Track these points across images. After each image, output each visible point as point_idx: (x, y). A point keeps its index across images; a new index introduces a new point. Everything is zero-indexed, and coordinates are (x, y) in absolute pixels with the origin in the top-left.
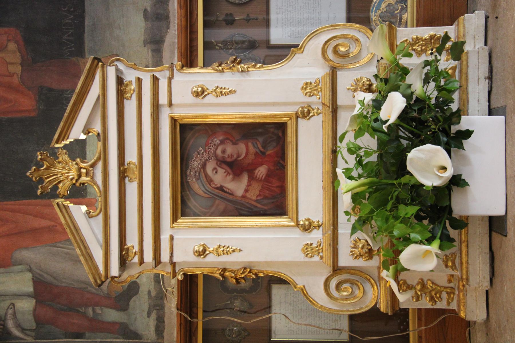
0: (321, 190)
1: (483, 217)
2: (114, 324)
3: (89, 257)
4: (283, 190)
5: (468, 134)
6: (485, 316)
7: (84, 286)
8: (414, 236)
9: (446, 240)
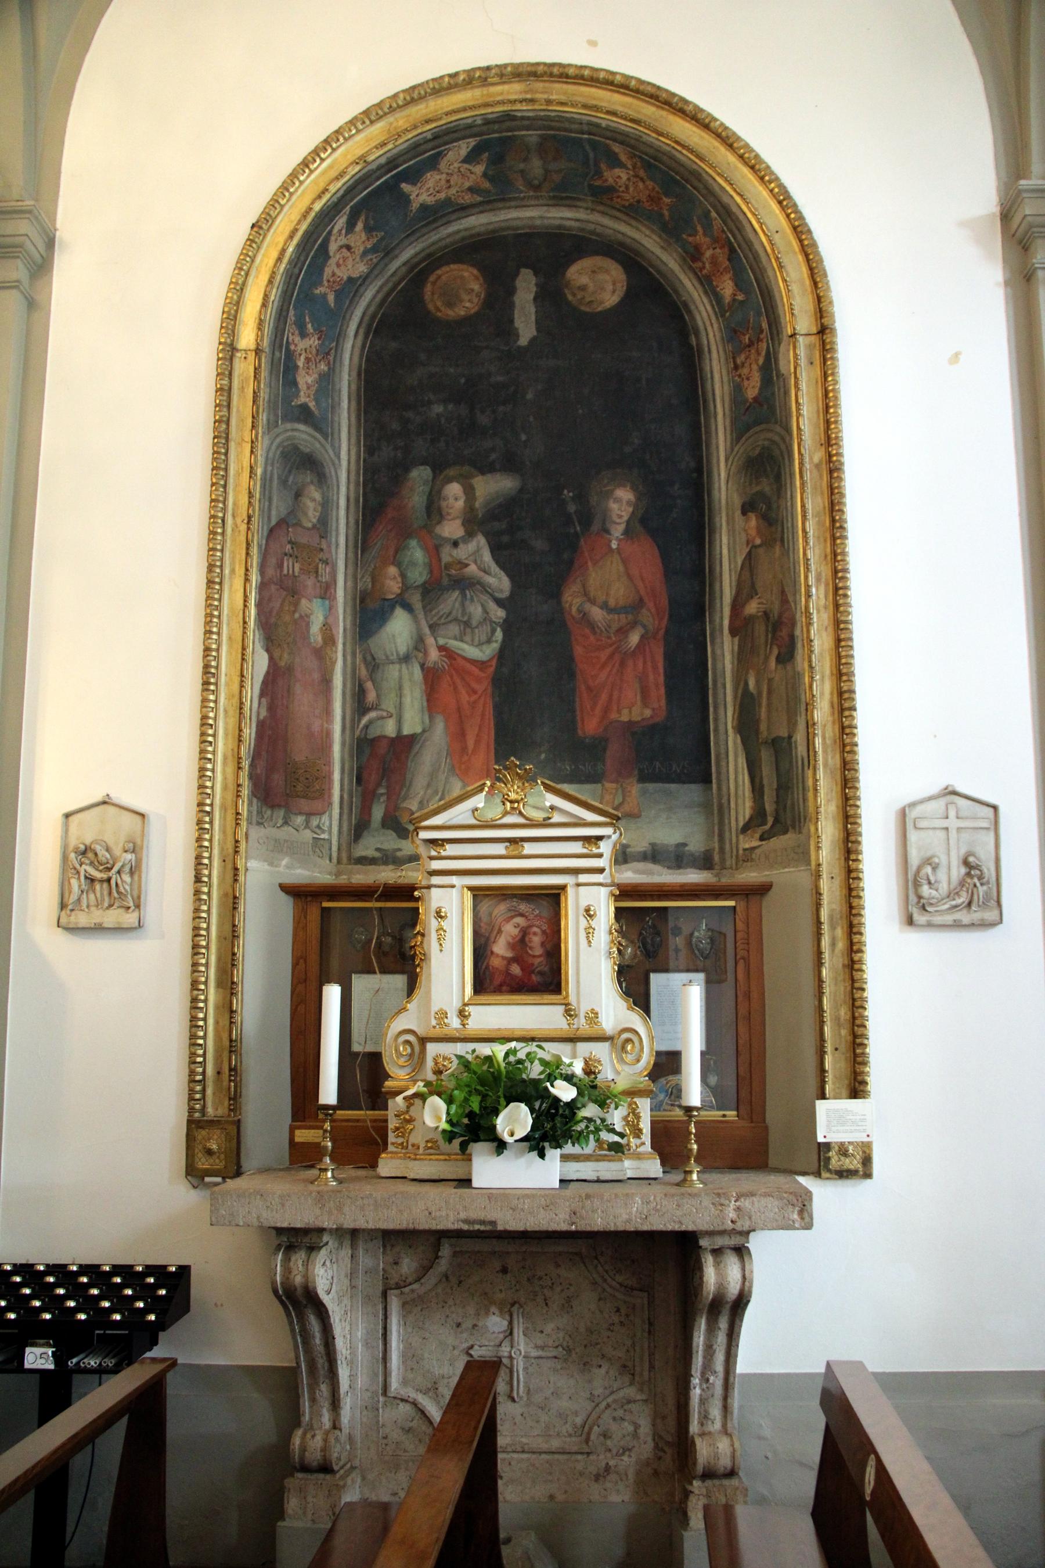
0: (497, 1027)
1: (470, 1173)
4: (498, 990)
5: (542, 1155)
6: (383, 1175)
7: (407, 783)
8: (454, 1108)
9: (449, 1136)
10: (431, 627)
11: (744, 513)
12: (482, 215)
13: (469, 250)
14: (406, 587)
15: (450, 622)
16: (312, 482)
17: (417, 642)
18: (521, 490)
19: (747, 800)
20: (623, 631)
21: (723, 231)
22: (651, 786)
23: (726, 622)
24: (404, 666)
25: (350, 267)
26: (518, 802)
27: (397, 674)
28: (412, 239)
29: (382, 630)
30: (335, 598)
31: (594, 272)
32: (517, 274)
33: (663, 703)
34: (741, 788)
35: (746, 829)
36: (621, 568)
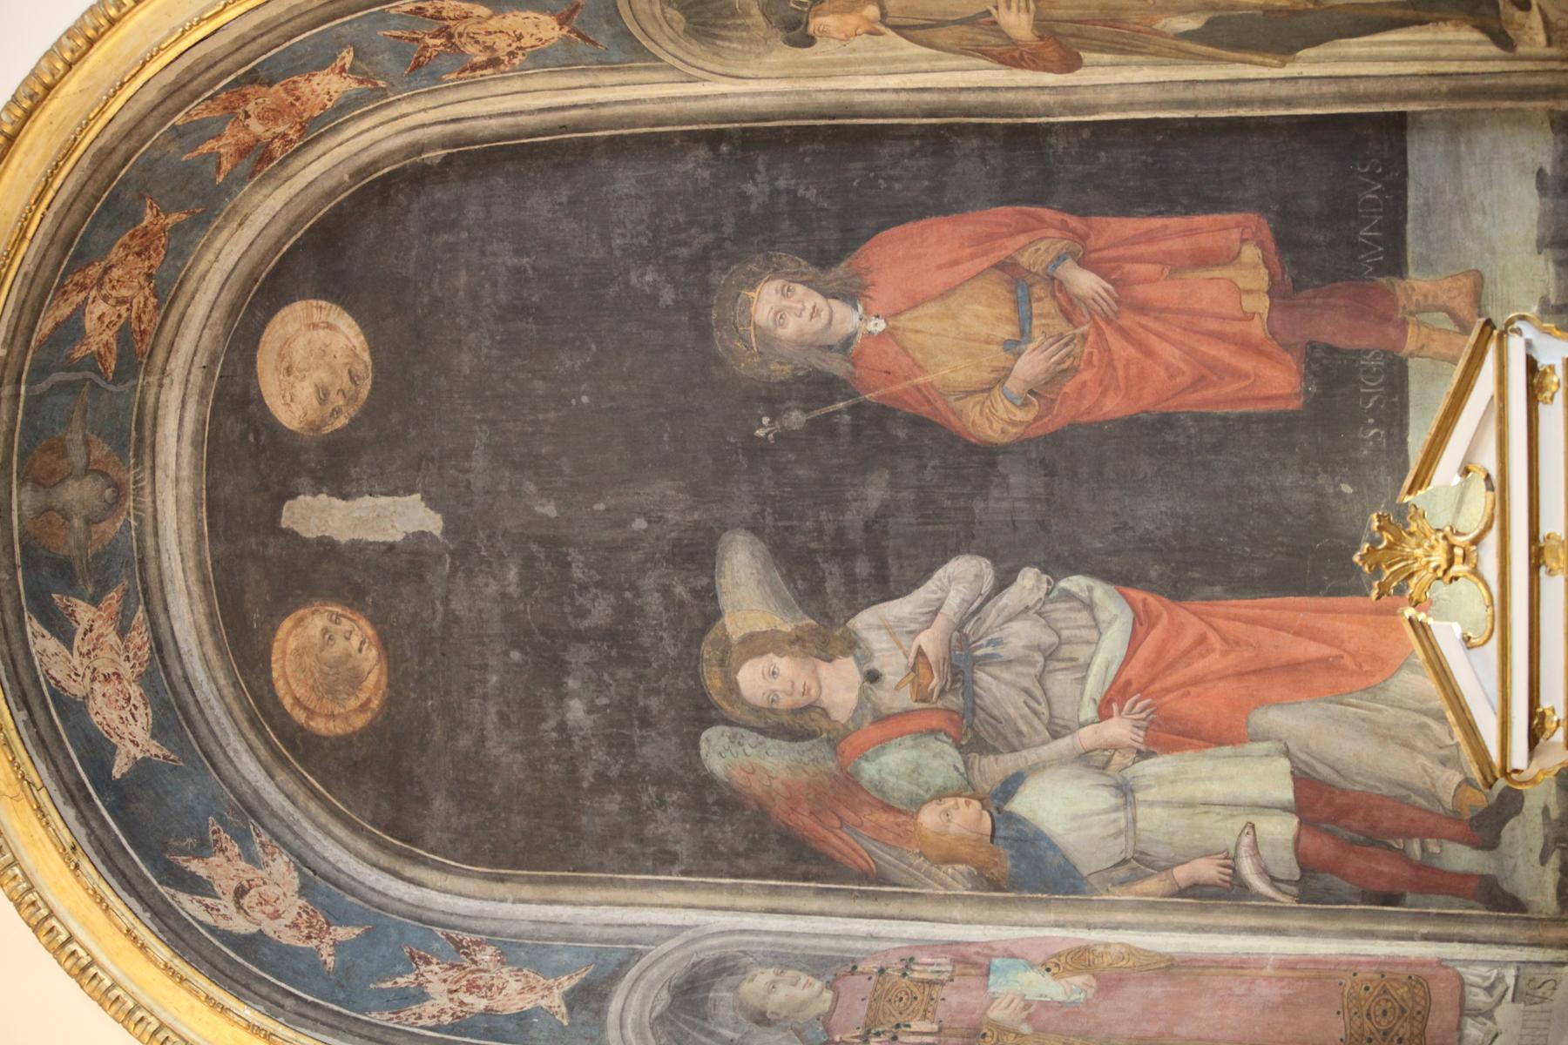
2: (1466, 876)
3: (1470, 730)
7: (1403, 792)
10: (1055, 736)
11: (808, 41)
12: (173, 610)
13: (244, 644)
14: (967, 789)
15: (1045, 692)
16: (734, 988)
17: (1088, 766)
18: (755, 529)
19: (1442, 37)
20: (1070, 307)
21: (211, 98)
22: (1413, 248)
23: (1049, 79)
24: (1140, 796)
25: (279, 891)
26: (1452, 547)
27: (1159, 812)
28: (220, 757)
29: (1058, 841)
30: (988, 945)
31: (289, 371)
32: (294, 535)
33: (1228, 218)
34: (1416, 50)
35: (1504, 41)
36: (930, 309)
